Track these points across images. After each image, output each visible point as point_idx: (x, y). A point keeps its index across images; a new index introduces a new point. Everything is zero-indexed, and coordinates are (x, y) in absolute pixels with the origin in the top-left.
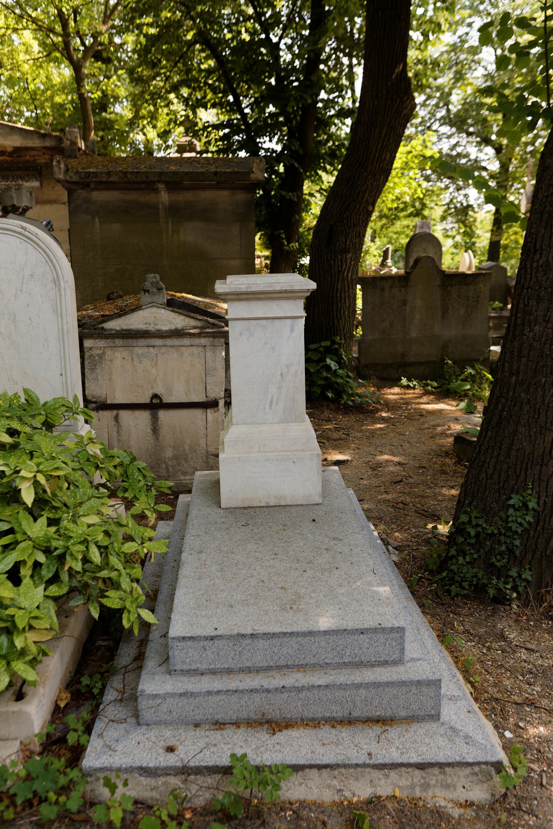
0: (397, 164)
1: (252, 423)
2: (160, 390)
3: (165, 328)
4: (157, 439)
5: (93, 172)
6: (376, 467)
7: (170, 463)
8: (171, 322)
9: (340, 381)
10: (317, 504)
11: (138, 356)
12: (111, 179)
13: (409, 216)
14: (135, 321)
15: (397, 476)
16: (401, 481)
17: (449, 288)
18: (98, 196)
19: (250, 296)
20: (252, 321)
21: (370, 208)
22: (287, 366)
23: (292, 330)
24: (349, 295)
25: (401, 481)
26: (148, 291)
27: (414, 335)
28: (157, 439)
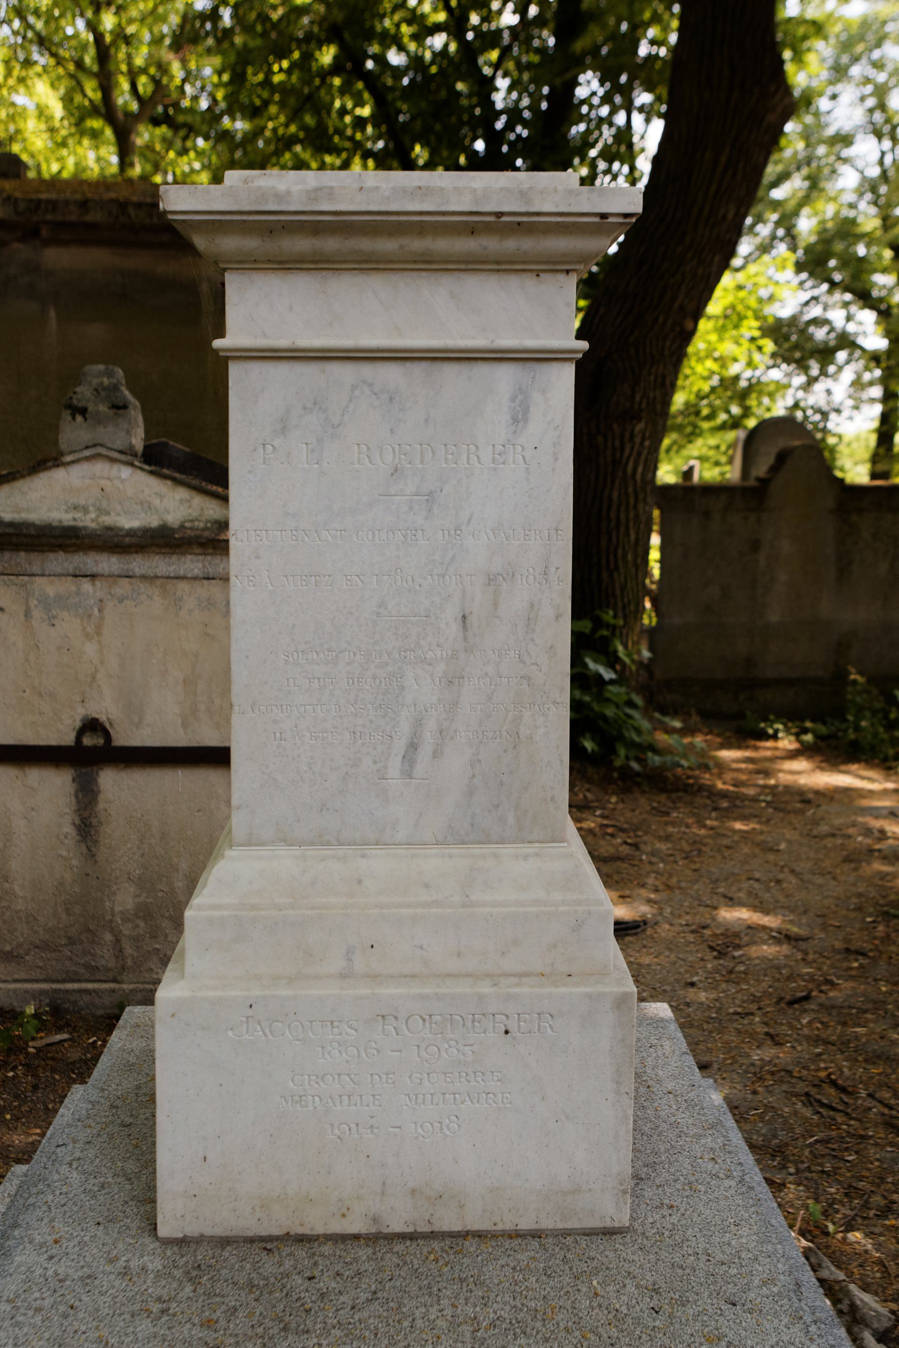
0: (714, 308)
1: (320, 840)
2: (105, 707)
3: (129, 523)
4: (91, 855)
5: (49, 201)
6: (727, 943)
7: (126, 929)
8: (147, 507)
9: (610, 712)
10: (609, 1232)
11: (46, 604)
12: (89, 218)
13: (723, 427)
14: (43, 498)
15: (790, 978)
16: (807, 998)
17: (854, 518)
18: (60, 258)
19: (331, 244)
20: (337, 370)
21: (689, 325)
22: (491, 580)
23: (520, 417)
24: (637, 516)
25: (807, 998)
26: (83, 411)
27: (774, 617)
28: (91, 855)
